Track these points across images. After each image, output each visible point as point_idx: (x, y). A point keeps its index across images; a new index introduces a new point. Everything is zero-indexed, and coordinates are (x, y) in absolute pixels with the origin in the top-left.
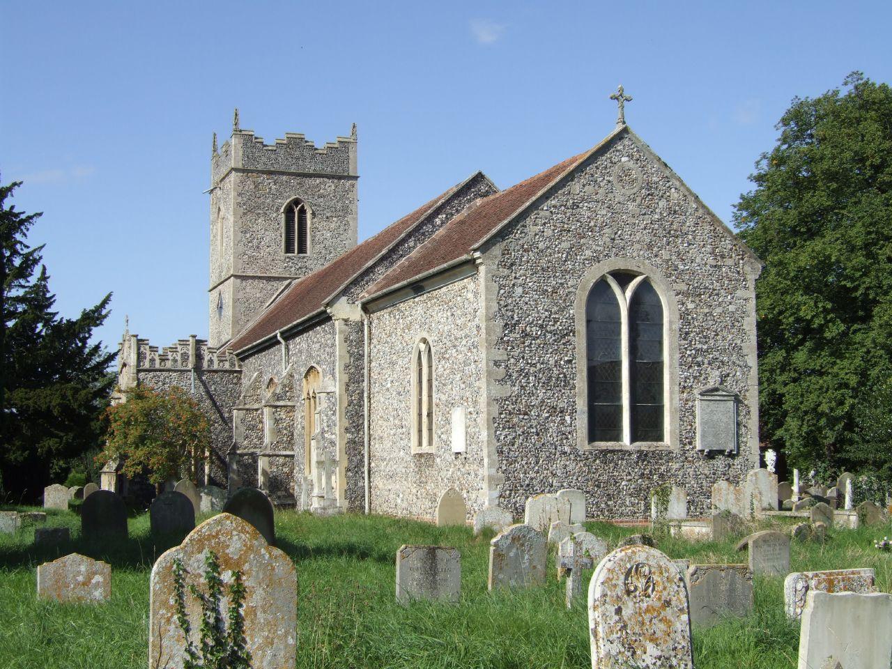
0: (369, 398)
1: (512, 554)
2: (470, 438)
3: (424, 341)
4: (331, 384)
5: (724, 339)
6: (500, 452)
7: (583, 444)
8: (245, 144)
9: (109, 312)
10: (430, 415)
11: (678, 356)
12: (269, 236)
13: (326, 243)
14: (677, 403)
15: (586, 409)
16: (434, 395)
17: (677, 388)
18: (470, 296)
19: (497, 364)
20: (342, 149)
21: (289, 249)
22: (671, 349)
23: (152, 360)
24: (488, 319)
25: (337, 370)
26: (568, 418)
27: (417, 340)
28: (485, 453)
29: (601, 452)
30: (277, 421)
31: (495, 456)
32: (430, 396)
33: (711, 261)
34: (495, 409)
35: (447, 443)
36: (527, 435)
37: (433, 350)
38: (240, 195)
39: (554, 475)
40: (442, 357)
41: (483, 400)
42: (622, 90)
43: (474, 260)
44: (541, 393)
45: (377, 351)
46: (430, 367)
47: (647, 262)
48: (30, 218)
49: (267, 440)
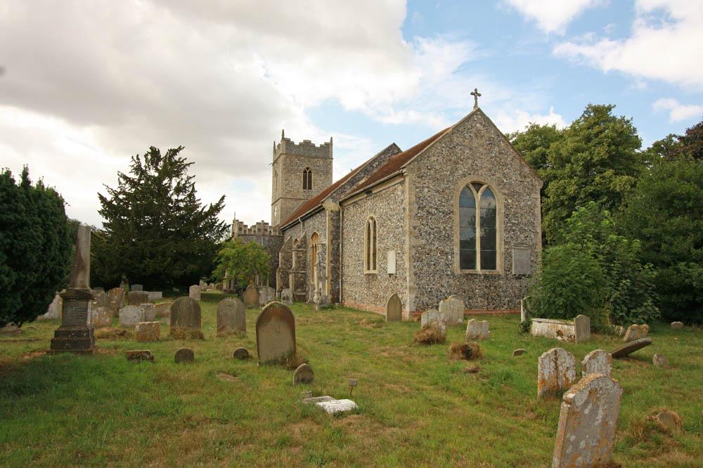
0: (342, 247)
1: (587, 411)
2: (398, 266)
3: (372, 218)
4: (325, 239)
5: (526, 218)
6: (415, 274)
7: (458, 271)
8: (287, 144)
9: (223, 207)
10: (374, 254)
11: (503, 226)
12: (297, 182)
13: (318, 187)
14: (503, 250)
15: (459, 252)
16: (377, 245)
17: (503, 243)
18: (399, 193)
19: (415, 228)
20: (327, 147)
21: (305, 188)
22: (500, 223)
23: (245, 231)
24: (410, 204)
25: (327, 234)
26: (450, 257)
27: (368, 218)
28: (407, 274)
29: (466, 274)
30: (299, 257)
31: (413, 276)
32: (374, 245)
33: (519, 179)
34: (414, 251)
35: (385, 269)
36: (429, 265)
37: (377, 222)
38: (284, 165)
39: (442, 286)
40: (382, 225)
41: (406, 247)
42: (476, 90)
43: (402, 174)
44: (437, 244)
45: (348, 225)
46: (375, 231)
47: (489, 178)
48: (189, 165)
49: (294, 266)
